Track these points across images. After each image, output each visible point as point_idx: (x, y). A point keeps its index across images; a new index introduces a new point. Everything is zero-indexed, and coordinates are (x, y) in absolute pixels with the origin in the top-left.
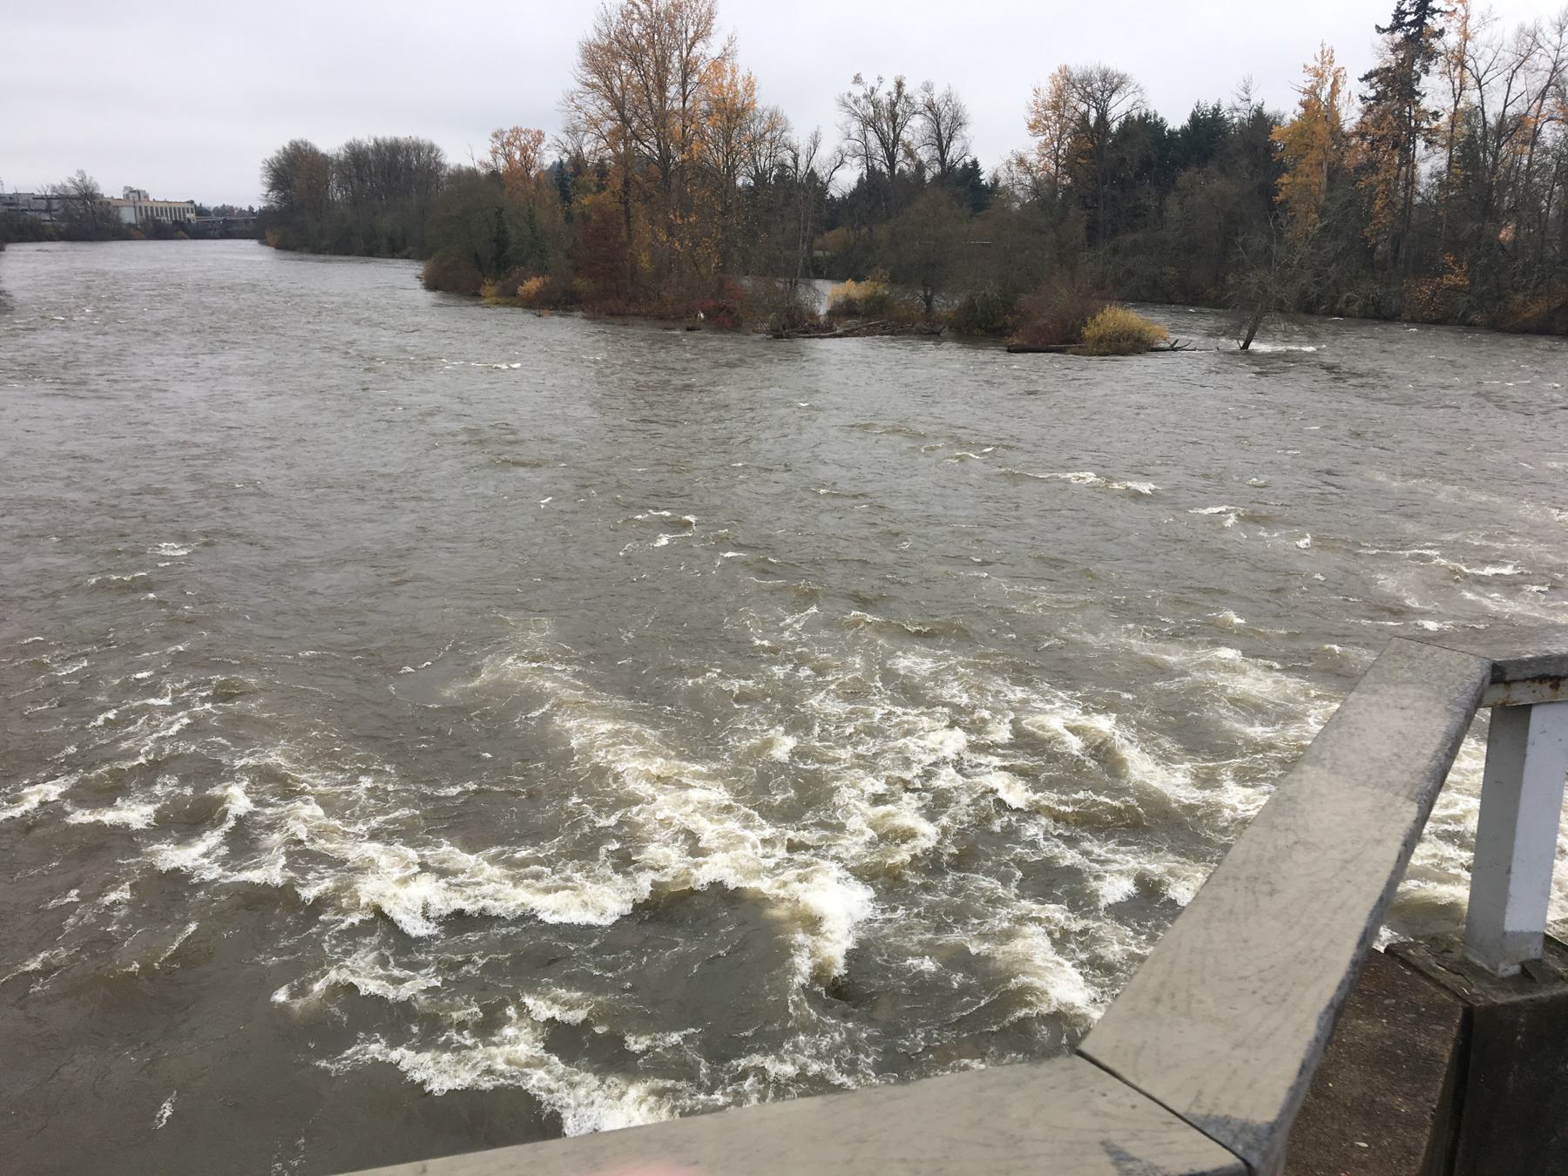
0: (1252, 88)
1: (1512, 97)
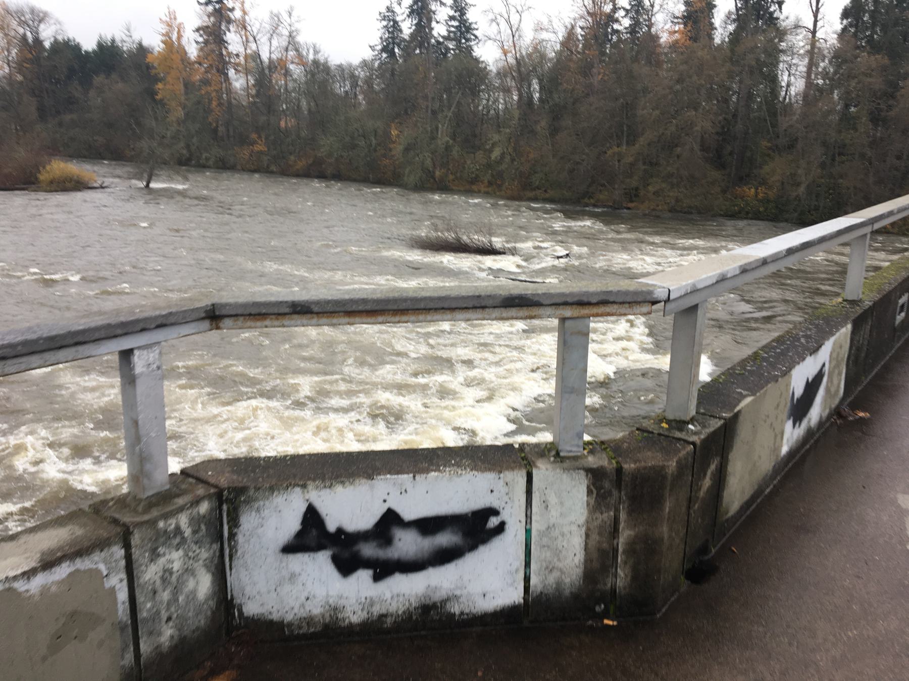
0: (132, 29)
1: (514, 30)
